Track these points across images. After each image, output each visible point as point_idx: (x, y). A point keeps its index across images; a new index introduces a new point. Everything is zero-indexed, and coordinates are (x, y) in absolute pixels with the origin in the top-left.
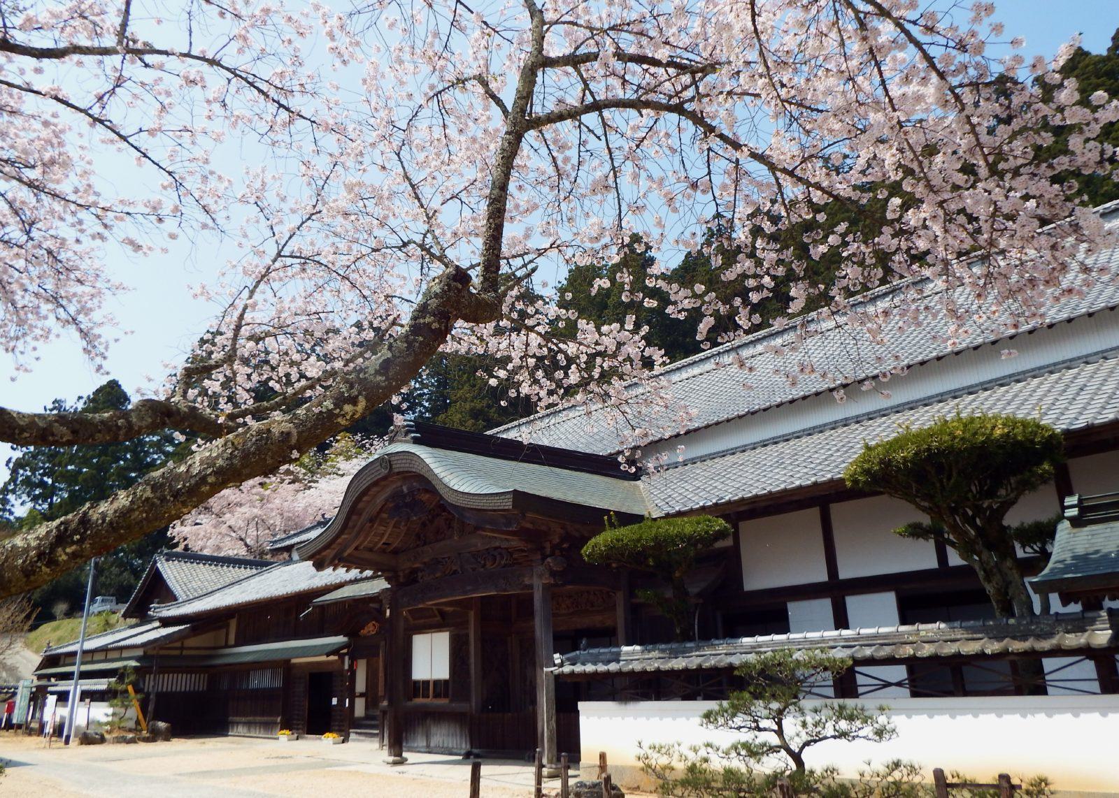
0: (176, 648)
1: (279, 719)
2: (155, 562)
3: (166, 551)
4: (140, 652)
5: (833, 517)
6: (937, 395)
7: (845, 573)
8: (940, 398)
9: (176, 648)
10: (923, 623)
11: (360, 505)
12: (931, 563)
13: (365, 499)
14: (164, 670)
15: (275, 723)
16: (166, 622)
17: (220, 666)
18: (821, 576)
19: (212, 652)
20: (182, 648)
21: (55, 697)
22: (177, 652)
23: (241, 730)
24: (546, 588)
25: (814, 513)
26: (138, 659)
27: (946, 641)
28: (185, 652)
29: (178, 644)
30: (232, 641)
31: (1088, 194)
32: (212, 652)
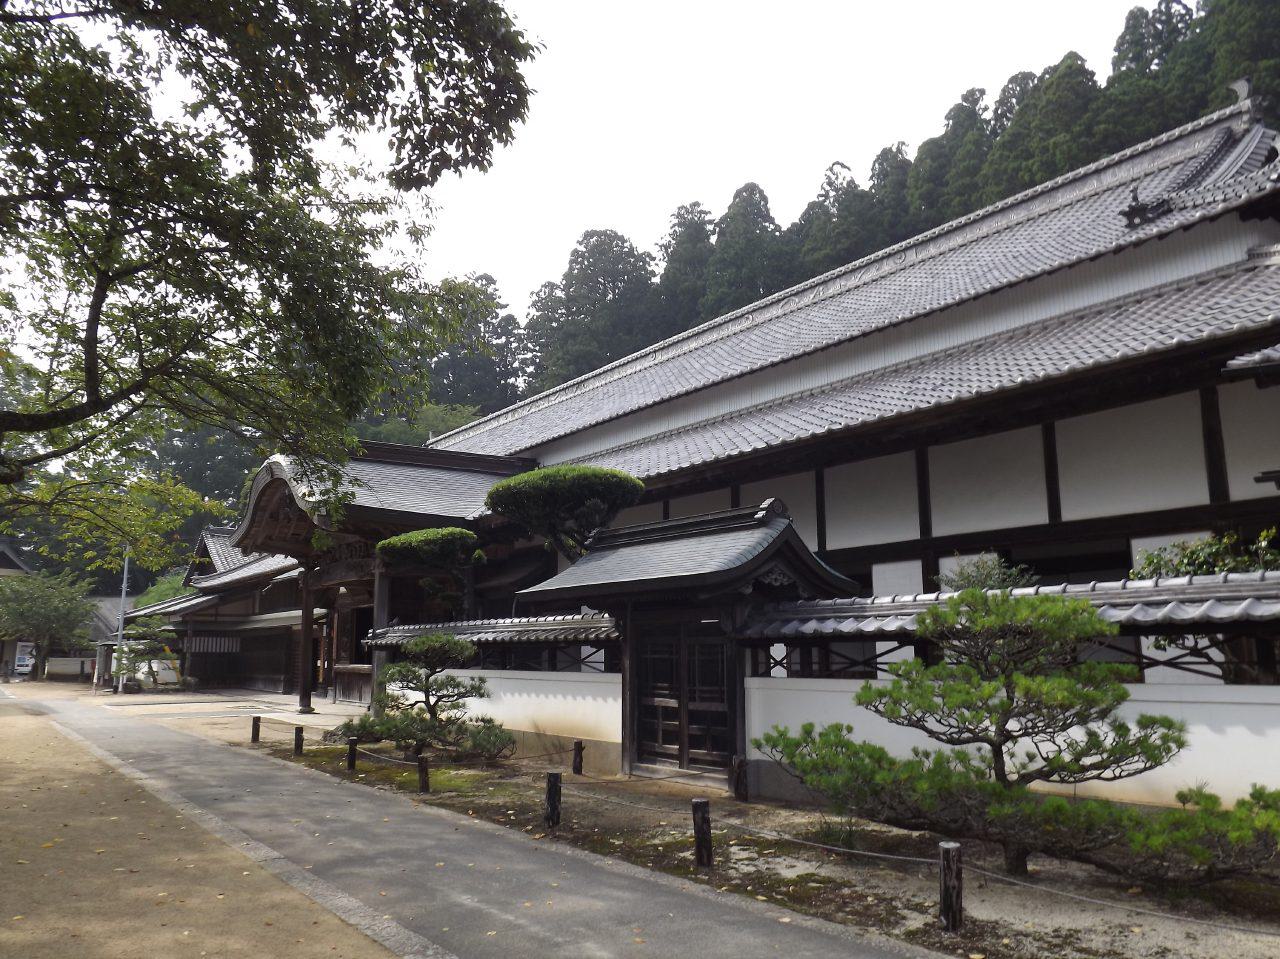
0: (212, 615)
1: (282, 678)
2: (202, 540)
3: (211, 527)
4: (179, 619)
5: (931, 469)
6: (1153, 289)
7: (939, 530)
8: (1156, 292)
9: (212, 615)
10: (1071, 582)
11: (262, 504)
12: (1040, 517)
13: (264, 498)
14: (197, 633)
15: (279, 681)
16: (205, 591)
17: (251, 630)
18: (914, 534)
19: (241, 619)
20: (217, 615)
21: (383, 654)
22: (213, 618)
23: (261, 686)
24: (381, 574)
25: (908, 458)
26: (175, 624)
27: (1183, 602)
28: (220, 619)
29: (212, 611)
30: (257, 611)
31: (1157, 72)
32: (241, 619)
